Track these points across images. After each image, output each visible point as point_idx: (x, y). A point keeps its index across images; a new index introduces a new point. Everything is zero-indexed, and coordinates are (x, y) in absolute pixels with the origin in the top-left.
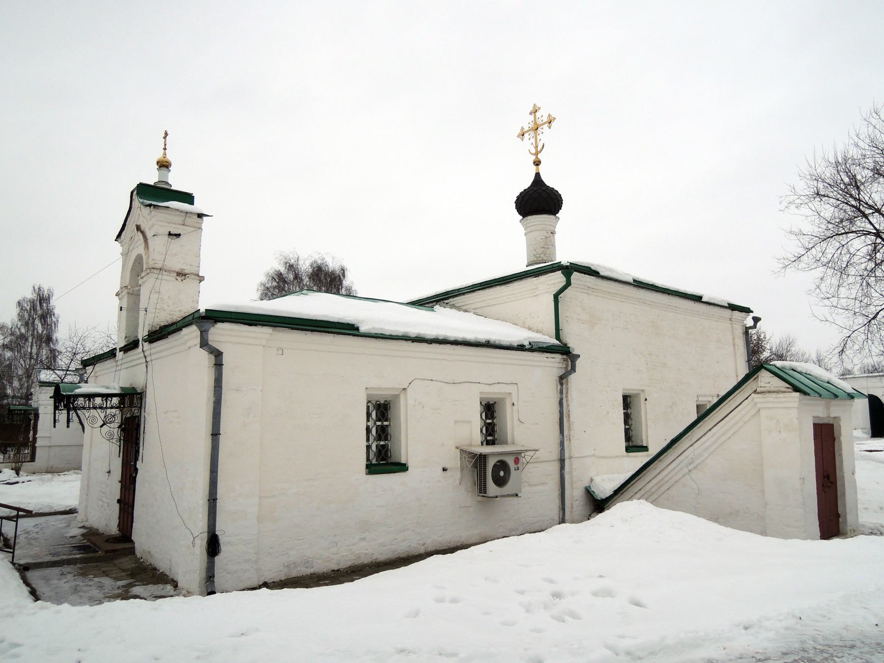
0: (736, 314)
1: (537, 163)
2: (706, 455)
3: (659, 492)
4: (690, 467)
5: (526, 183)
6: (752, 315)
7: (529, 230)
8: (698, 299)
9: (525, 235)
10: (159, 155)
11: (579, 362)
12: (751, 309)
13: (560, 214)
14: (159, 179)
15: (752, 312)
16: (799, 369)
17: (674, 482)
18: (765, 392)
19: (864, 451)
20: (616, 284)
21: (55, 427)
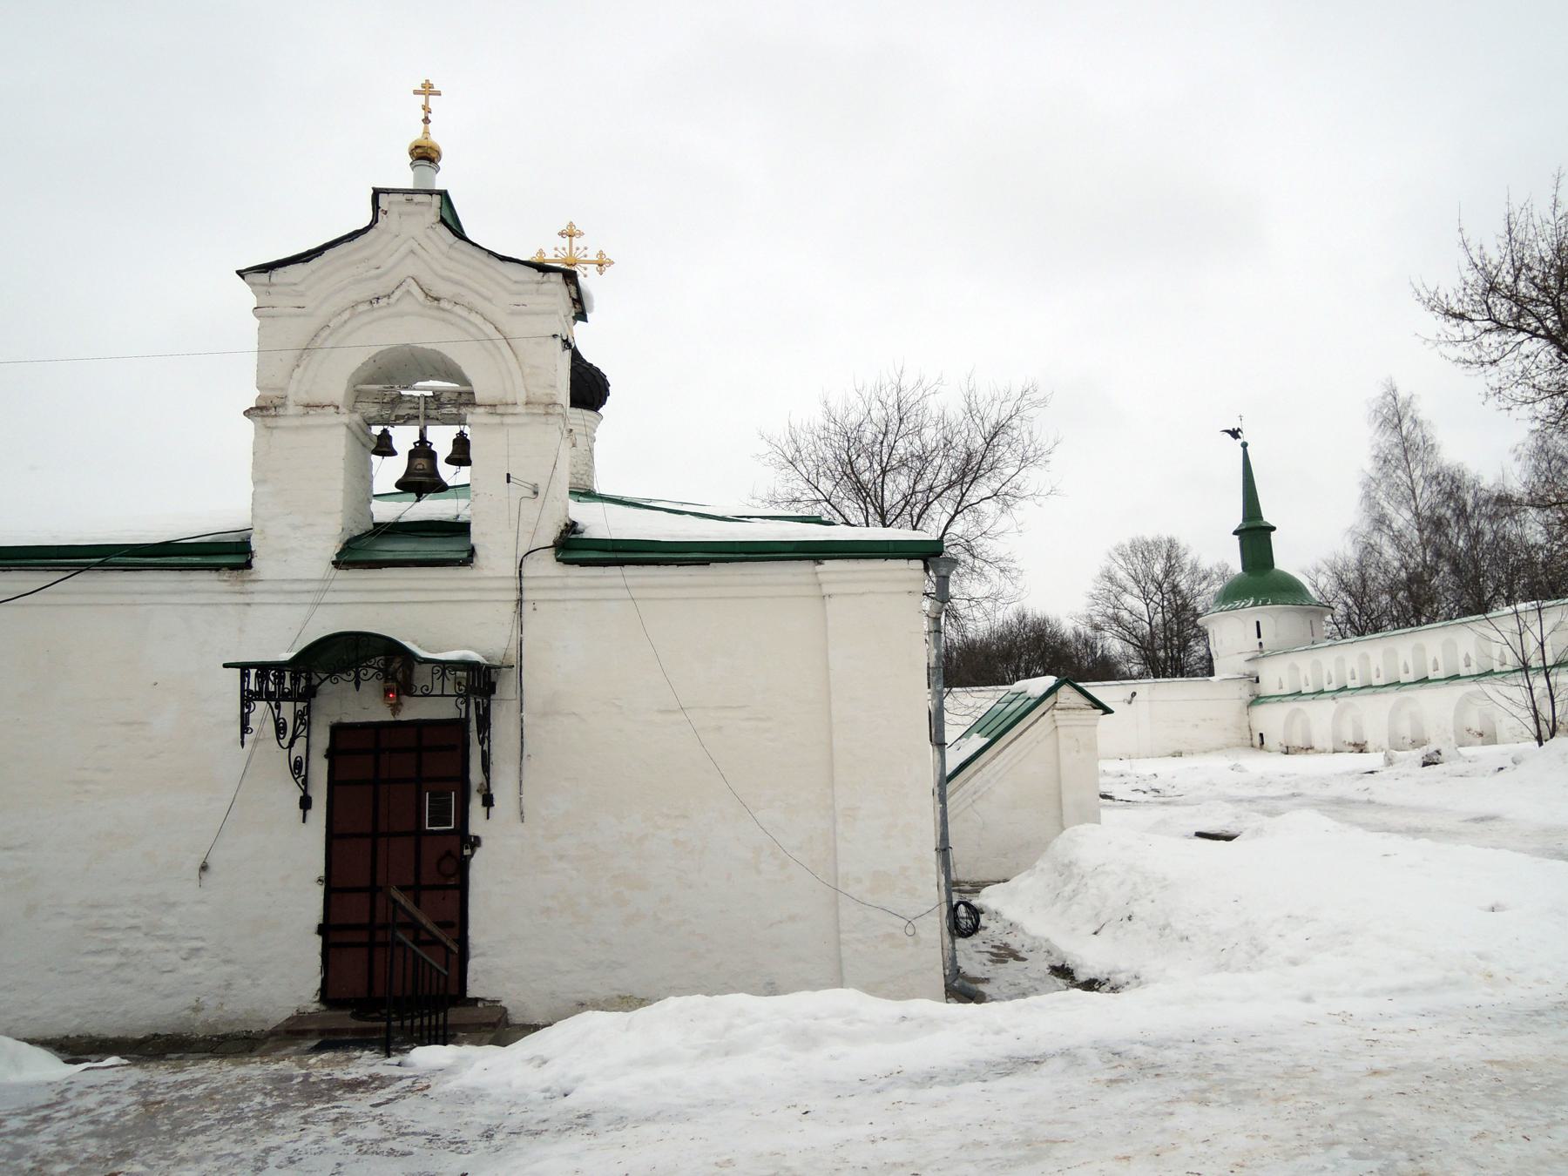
4: (975, 797)
10: (415, 134)
14: (415, 183)
21: (226, 666)
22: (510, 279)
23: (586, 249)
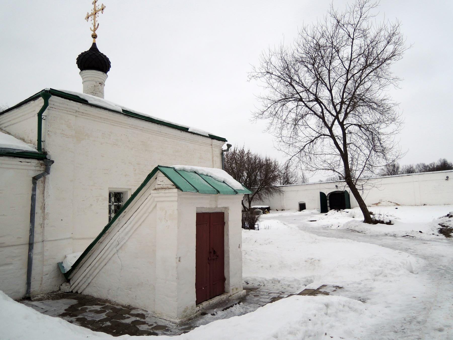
0: (215, 141)
1: (94, 36)
2: (127, 239)
3: (100, 267)
4: (118, 248)
5: (87, 47)
6: (226, 143)
7: (84, 80)
8: (185, 130)
9: (83, 83)
11: (53, 168)
12: (226, 139)
13: (108, 73)
15: (227, 141)
16: (200, 172)
17: (108, 260)
18: (160, 189)
19: (310, 221)
20: (107, 112)
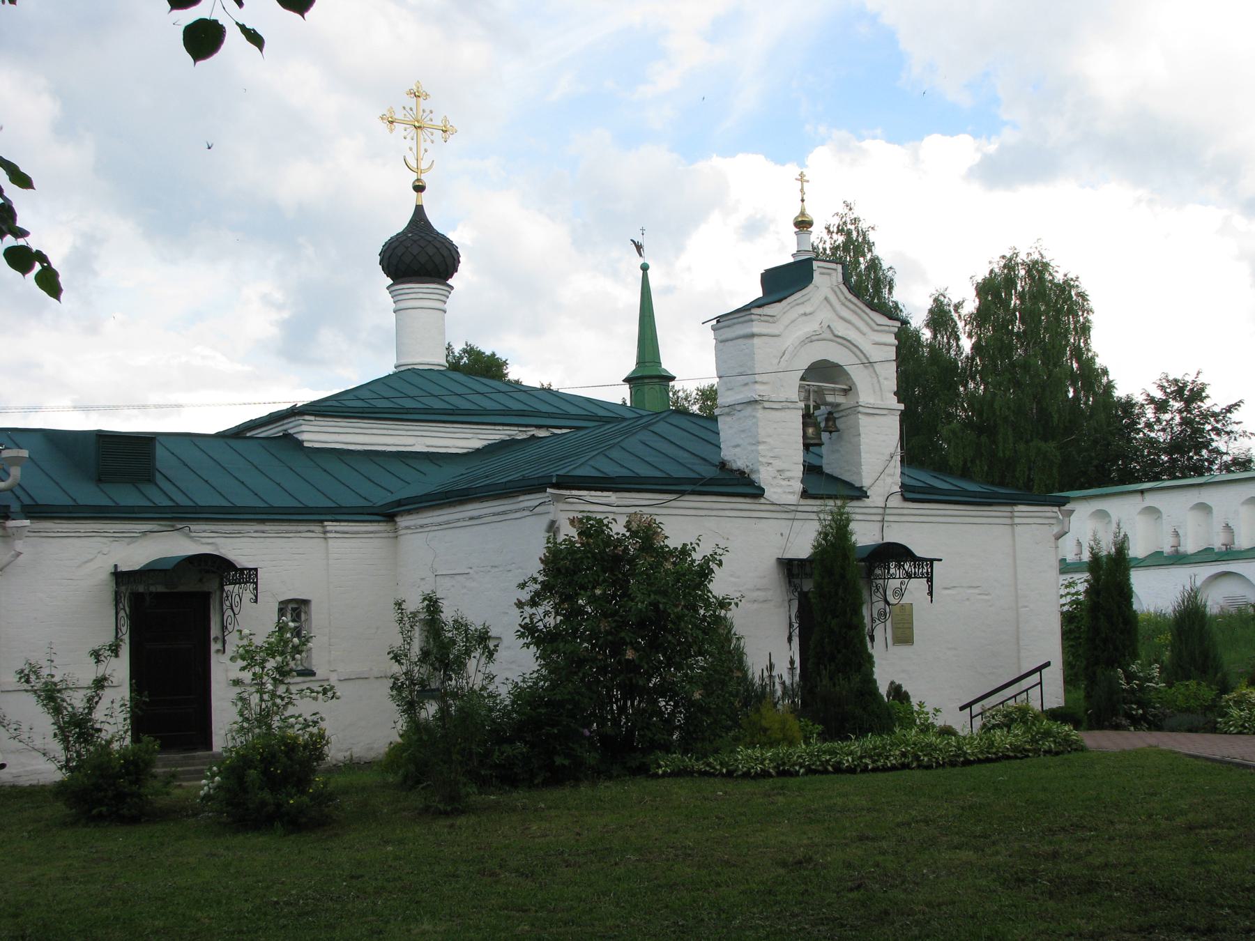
22: (875, 322)
23: (431, 112)
